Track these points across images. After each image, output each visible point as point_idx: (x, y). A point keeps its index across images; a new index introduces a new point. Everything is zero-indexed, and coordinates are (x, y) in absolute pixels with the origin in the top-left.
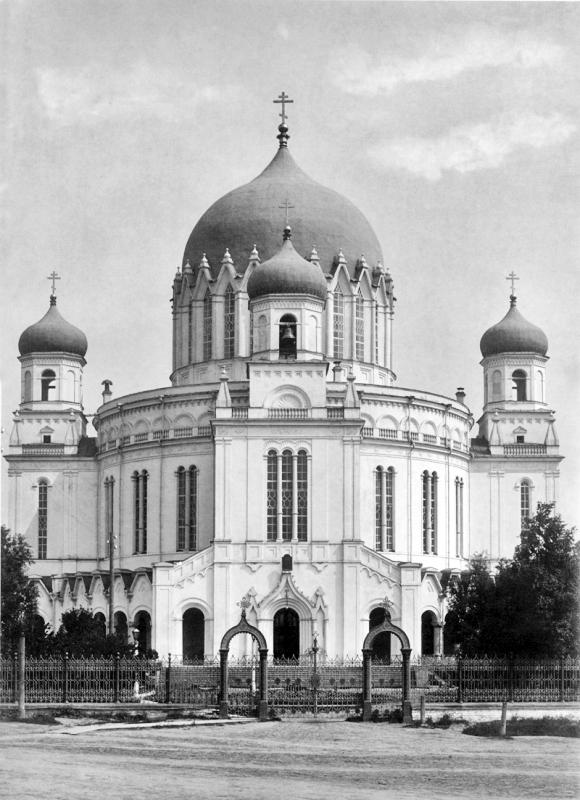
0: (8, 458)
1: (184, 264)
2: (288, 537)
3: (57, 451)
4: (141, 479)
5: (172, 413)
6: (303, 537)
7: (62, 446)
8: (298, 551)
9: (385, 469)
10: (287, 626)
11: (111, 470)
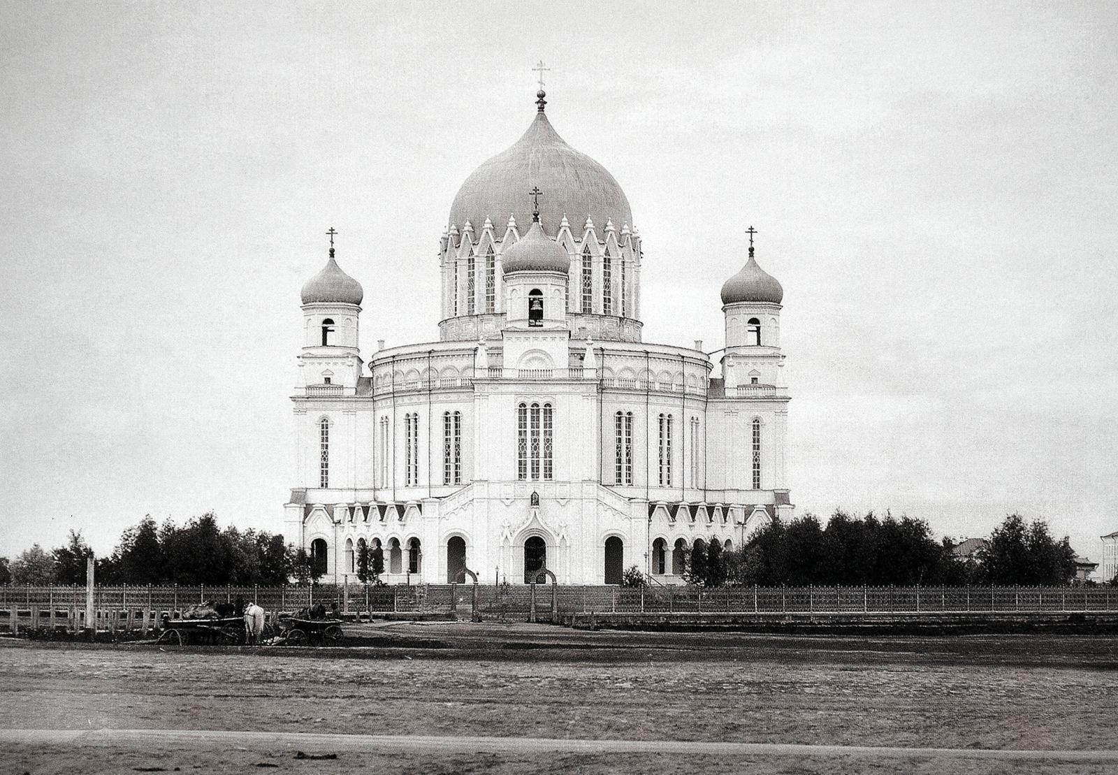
0: (293, 399)
1: (450, 225)
2: (535, 476)
3: (337, 392)
4: (412, 420)
5: (439, 364)
6: (549, 475)
7: (342, 387)
8: (543, 487)
9: (625, 414)
10: (535, 550)
11: (385, 409)
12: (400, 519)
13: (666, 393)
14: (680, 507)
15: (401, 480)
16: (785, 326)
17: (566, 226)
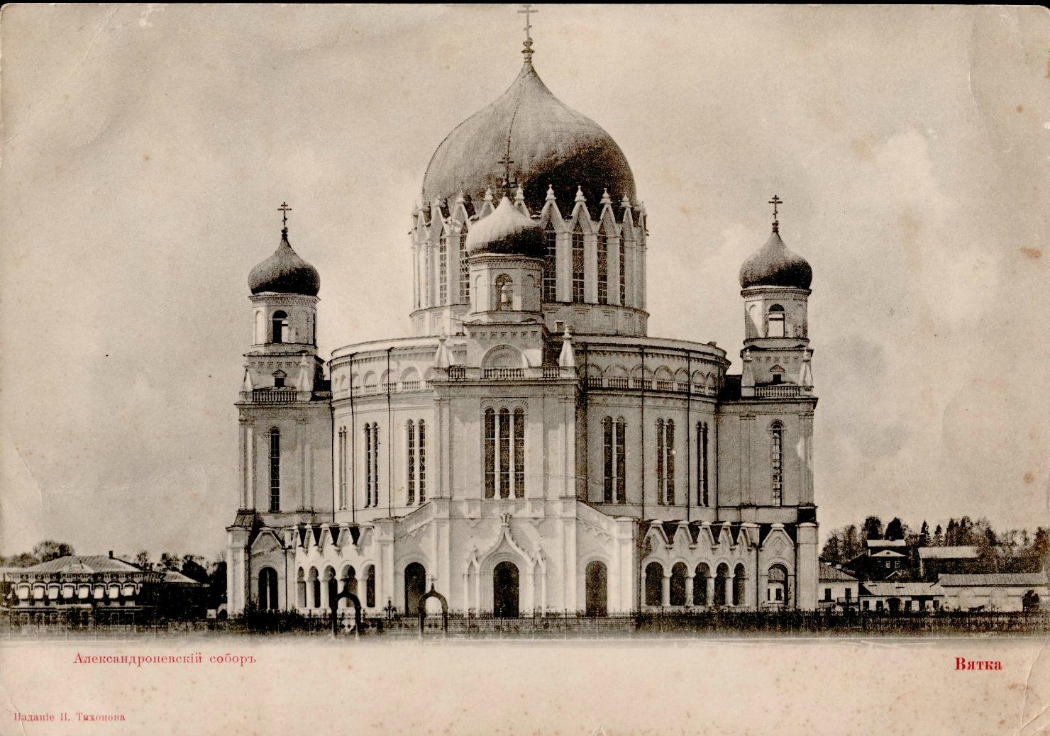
12: (355, 543)
13: (663, 392)
14: (652, 526)
15: (651, 498)
16: (821, 309)
17: (581, 201)
